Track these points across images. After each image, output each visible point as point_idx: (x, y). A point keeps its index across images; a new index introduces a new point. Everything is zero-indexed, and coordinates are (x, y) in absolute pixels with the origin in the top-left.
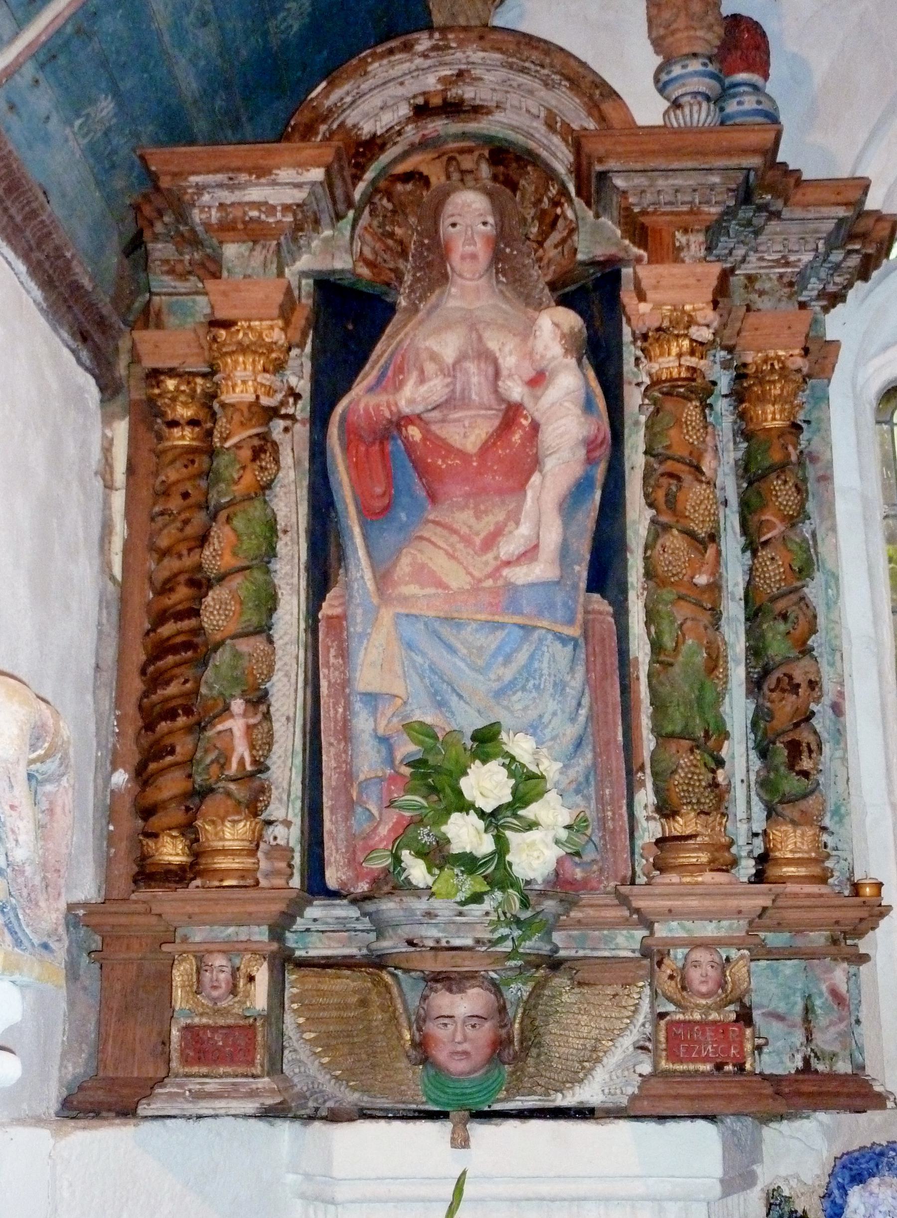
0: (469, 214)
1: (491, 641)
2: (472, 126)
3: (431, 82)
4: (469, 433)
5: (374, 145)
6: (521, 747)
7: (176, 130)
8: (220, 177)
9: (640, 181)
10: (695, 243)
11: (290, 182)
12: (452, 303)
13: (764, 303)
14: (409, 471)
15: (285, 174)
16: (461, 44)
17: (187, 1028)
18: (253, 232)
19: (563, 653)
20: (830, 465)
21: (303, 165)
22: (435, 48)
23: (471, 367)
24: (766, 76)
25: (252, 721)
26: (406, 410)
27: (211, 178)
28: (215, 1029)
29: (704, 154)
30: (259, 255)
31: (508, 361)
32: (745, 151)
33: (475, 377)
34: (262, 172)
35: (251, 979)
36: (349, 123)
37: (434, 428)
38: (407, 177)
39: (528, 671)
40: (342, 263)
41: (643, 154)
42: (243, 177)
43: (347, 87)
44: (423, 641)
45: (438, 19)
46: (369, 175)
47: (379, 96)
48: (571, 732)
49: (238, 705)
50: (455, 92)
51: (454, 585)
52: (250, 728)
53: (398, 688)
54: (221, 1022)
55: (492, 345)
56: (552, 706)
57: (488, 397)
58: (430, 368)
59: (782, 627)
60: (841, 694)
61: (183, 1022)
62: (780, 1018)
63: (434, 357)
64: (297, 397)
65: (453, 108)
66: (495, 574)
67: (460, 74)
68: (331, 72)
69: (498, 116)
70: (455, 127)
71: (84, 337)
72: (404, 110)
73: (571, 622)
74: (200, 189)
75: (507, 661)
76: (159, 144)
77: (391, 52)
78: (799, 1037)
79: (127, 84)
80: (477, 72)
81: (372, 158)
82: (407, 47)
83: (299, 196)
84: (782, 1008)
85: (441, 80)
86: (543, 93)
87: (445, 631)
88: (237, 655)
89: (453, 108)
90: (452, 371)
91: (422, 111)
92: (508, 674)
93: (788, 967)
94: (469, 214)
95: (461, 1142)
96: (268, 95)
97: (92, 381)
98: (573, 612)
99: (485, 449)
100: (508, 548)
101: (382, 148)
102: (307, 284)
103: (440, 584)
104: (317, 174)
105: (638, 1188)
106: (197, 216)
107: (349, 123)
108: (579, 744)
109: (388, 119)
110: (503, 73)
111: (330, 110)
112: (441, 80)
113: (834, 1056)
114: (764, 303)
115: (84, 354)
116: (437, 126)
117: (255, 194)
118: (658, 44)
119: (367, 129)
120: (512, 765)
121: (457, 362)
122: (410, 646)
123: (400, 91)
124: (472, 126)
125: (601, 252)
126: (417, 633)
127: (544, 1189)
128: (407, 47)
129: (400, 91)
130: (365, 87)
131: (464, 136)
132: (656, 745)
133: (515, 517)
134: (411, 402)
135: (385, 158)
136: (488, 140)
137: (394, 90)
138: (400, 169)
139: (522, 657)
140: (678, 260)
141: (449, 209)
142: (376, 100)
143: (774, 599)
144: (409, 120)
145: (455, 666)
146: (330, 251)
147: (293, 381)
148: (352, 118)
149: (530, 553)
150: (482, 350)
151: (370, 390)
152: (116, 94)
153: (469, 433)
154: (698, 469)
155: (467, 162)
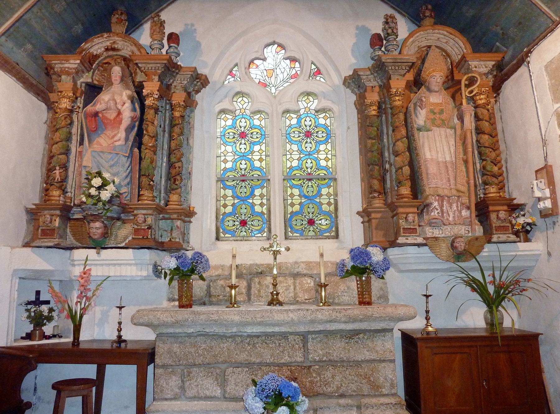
0: (117, 71)
1: (110, 156)
2: (118, 53)
3: (108, 43)
4: (111, 115)
5: (97, 57)
6: (106, 175)
7: (52, 51)
8: (58, 62)
9: (144, 65)
10: (156, 78)
11: (73, 63)
12: (112, 89)
13: (177, 91)
14: (96, 123)
15: (71, 61)
16: (113, 36)
17: (42, 230)
18: (68, 74)
19: (125, 159)
20: (193, 125)
21: (75, 60)
22: (108, 36)
23: (111, 102)
24: (178, 45)
25: (61, 171)
26: (98, 110)
27: (56, 62)
28: (47, 230)
29: (156, 60)
30: (69, 78)
31: (118, 101)
32: (163, 60)
33: (112, 103)
34: (67, 61)
35: (55, 220)
36: (91, 51)
37: (104, 114)
38: (106, 63)
39: (117, 162)
40: (90, 80)
41: (143, 59)
42: (63, 62)
43: (89, 44)
44: (96, 156)
45: (113, 30)
46: (96, 63)
47: (97, 46)
48: (125, 174)
49: (57, 168)
50: (113, 46)
51: (104, 145)
52: (60, 172)
53: (90, 165)
54: (48, 228)
55: (116, 98)
56: (121, 169)
57: (115, 108)
58: (102, 102)
59: (174, 156)
60: (191, 171)
61: (41, 228)
62: (166, 231)
63: (103, 100)
64: (79, 108)
65: (114, 49)
66: (113, 143)
67: (114, 42)
68: (86, 40)
69: (123, 51)
70: (115, 53)
71: (39, 95)
72: (103, 49)
73: (126, 153)
74: (56, 64)
75: (113, 160)
76: (47, 54)
77: (99, 37)
78: (169, 235)
79: (33, 42)
80: (117, 42)
81: (97, 59)
82: (102, 36)
83: (76, 66)
84: (167, 229)
85: (110, 43)
86: (130, 47)
87: (101, 154)
88: (58, 158)
89: (114, 49)
90: (107, 103)
91: (107, 49)
92: (112, 163)
93: (169, 221)
94: (117, 71)
95: (98, 253)
96: (72, 45)
97: (44, 104)
98: (127, 151)
99: (114, 119)
100: (116, 138)
101: (99, 57)
102: (83, 85)
103: (101, 145)
104: (78, 62)
105: (134, 262)
106: (56, 70)
107: (91, 51)
108: (127, 177)
109: (99, 51)
110: (123, 42)
111: (86, 49)
112: (110, 43)
113: (176, 238)
114: (177, 91)
115: (40, 98)
116: (111, 53)
117: (66, 65)
118: (151, 37)
119: (95, 53)
120: (103, 179)
121: (108, 101)
122: (94, 157)
123: (102, 45)
124: (118, 53)
125: (141, 80)
126: (95, 154)
127: (115, 262)
128: (102, 36)
129: (102, 45)
130: (93, 44)
131: (117, 55)
132: (142, 176)
133: (118, 132)
134: (98, 109)
135: (100, 59)
136: (122, 56)
137: (100, 45)
138: (105, 61)
139: (116, 160)
140: (152, 81)
141: (112, 70)
142: (96, 47)
143: (174, 150)
144: (104, 51)
145: (102, 161)
146: (86, 78)
147: (79, 104)
148: (91, 50)
149: (119, 140)
150: (117, 99)
151: (92, 106)
152: (31, 44)
153: (111, 115)
154: (153, 123)
155: (119, 60)
